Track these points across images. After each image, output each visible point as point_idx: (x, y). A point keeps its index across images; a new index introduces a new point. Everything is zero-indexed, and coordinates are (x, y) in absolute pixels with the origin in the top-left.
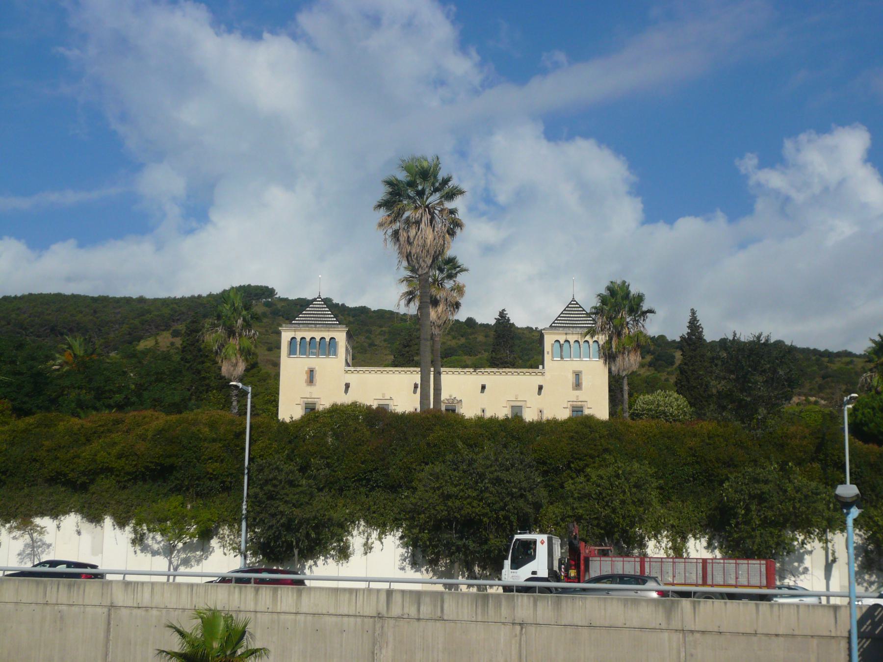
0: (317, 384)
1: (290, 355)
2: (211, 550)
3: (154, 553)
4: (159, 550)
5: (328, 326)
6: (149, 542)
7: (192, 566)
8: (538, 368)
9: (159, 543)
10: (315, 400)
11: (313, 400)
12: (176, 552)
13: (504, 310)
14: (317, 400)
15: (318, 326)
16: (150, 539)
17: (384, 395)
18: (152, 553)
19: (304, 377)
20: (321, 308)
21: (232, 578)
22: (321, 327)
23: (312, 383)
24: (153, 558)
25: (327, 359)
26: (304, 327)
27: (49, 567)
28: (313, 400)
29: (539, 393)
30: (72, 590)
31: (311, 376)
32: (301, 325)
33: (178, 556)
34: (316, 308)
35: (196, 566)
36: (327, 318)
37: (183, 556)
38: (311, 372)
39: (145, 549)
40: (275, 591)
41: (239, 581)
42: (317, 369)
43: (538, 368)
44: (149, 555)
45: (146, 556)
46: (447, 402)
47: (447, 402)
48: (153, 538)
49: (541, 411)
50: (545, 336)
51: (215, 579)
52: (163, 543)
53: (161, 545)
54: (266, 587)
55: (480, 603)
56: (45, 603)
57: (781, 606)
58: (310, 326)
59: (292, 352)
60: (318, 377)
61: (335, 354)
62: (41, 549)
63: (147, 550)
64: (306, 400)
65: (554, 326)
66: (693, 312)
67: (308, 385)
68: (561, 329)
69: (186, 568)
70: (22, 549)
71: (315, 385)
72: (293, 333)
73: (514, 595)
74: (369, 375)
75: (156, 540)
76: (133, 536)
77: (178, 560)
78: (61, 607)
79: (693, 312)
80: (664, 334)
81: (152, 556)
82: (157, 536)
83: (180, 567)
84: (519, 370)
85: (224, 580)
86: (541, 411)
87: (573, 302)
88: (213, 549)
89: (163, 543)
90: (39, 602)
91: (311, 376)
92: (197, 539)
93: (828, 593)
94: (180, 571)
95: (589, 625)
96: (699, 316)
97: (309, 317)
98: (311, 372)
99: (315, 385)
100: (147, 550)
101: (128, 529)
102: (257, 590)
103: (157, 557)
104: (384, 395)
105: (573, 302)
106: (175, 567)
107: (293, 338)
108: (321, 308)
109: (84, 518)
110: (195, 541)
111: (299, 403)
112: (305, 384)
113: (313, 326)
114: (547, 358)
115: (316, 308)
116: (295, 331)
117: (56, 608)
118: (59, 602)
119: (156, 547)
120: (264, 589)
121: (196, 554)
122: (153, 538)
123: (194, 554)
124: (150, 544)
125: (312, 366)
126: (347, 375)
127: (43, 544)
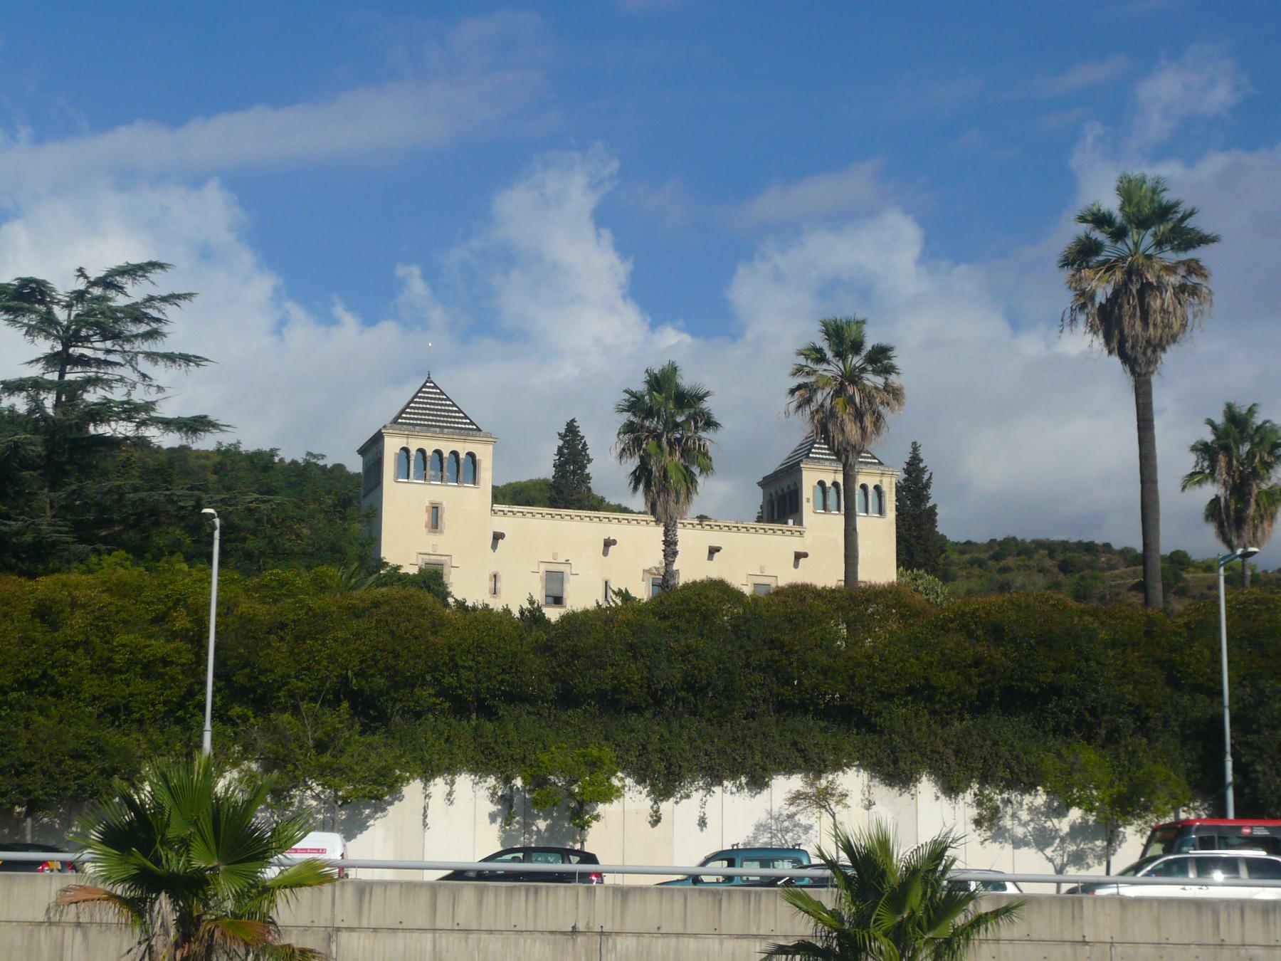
0: (445, 530)
1: (397, 478)
2: (1121, 837)
3: (1018, 843)
4: (1025, 837)
5: (463, 431)
6: (1007, 822)
7: (1089, 866)
8: (786, 523)
9: (1026, 824)
10: (443, 558)
11: (439, 558)
12: (1058, 841)
13: (573, 421)
14: (446, 558)
15: (446, 430)
16: (1008, 817)
17: (555, 556)
18: (1013, 842)
19: (424, 517)
20: (434, 399)
21: (575, 873)
22: (452, 434)
23: (437, 528)
24: (1017, 851)
25: (461, 489)
26: (423, 431)
27: (579, 862)
28: (439, 558)
29: (494, 546)
30: (1271, 920)
31: (435, 517)
32: (417, 428)
33: (1063, 849)
34: (427, 398)
35: (1096, 865)
36: (432, 415)
37: (1072, 848)
38: (435, 510)
39: (999, 834)
40: (481, 892)
41: (481, 876)
42: (445, 504)
43: (786, 523)
44: (1008, 847)
45: (1002, 848)
46: (656, 572)
47: (656, 572)
48: (1014, 816)
49: (495, 576)
50: (804, 473)
51: (680, 877)
52: (1032, 825)
53: (1030, 828)
54: (565, 887)
55: (619, 898)
56: (1220, 942)
57: (1076, 905)
58: (432, 429)
59: (404, 471)
60: (446, 517)
61: (474, 480)
62: (791, 834)
63: (1004, 837)
64: (427, 557)
65: (402, 423)
66: (915, 447)
67: (429, 532)
68: (827, 463)
69: (1079, 869)
70: (751, 835)
71: (441, 532)
72: (404, 440)
73: (577, 887)
74: (533, 521)
75: (1020, 820)
76: (974, 812)
77: (1063, 856)
78: (1252, 951)
79: (915, 447)
80: (342, 463)
81: (1014, 848)
82: (1020, 813)
83: (1068, 868)
84: (563, 512)
85: (459, 875)
86: (495, 576)
87: (428, 384)
88: (1124, 837)
89: (1032, 825)
90: (1205, 941)
91: (435, 517)
92: (1094, 818)
93: (343, 863)
94: (1070, 873)
95: (1028, 938)
96: (923, 454)
97: (425, 414)
98: (435, 510)
99: (441, 532)
100: (1004, 837)
101: (969, 796)
102: (481, 892)
103: (1024, 850)
104: (555, 556)
105: (428, 384)
106: (1058, 868)
107: (406, 450)
108: (434, 399)
109: (875, 777)
110: (1091, 822)
111: (414, 562)
112: (425, 531)
113: (438, 430)
114: (807, 508)
115: (427, 398)
116: (408, 436)
117: (1242, 951)
118: (1248, 941)
119: (1020, 831)
120: (562, 890)
121: (1095, 845)
122: (1014, 816)
123: (1090, 845)
124: (1009, 827)
125: (437, 499)
126: (495, 518)
127: (795, 826)
